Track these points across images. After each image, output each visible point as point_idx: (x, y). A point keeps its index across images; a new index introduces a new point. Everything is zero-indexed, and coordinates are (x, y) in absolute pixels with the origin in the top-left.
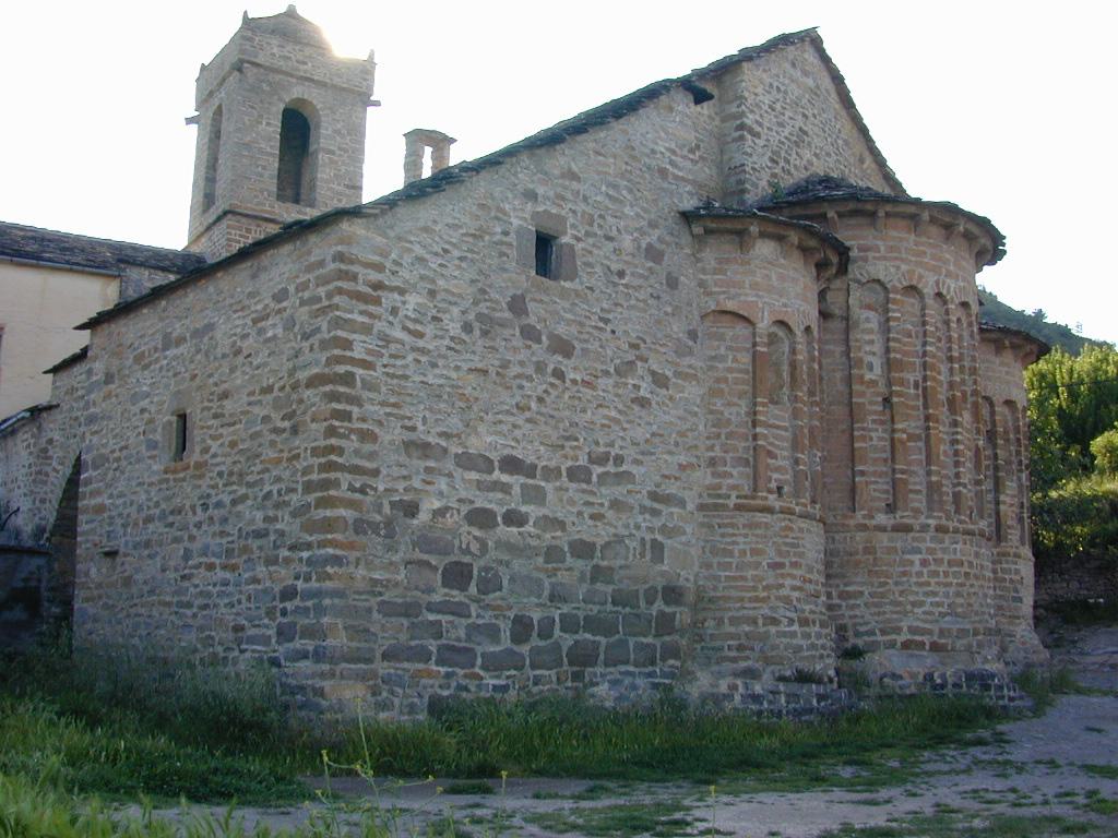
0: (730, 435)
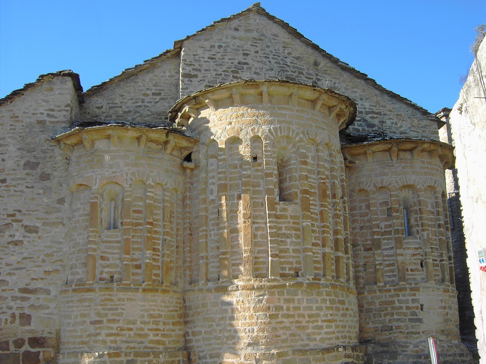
0: (79, 251)
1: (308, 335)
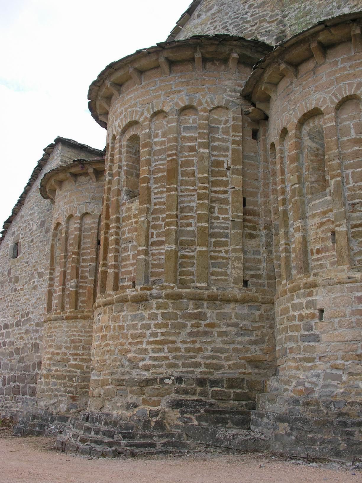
1: (130, 361)
